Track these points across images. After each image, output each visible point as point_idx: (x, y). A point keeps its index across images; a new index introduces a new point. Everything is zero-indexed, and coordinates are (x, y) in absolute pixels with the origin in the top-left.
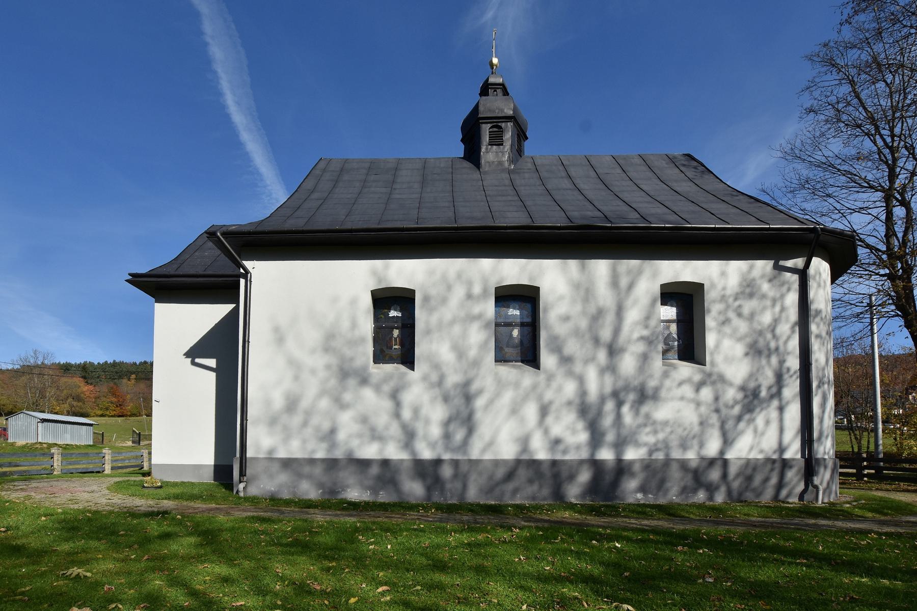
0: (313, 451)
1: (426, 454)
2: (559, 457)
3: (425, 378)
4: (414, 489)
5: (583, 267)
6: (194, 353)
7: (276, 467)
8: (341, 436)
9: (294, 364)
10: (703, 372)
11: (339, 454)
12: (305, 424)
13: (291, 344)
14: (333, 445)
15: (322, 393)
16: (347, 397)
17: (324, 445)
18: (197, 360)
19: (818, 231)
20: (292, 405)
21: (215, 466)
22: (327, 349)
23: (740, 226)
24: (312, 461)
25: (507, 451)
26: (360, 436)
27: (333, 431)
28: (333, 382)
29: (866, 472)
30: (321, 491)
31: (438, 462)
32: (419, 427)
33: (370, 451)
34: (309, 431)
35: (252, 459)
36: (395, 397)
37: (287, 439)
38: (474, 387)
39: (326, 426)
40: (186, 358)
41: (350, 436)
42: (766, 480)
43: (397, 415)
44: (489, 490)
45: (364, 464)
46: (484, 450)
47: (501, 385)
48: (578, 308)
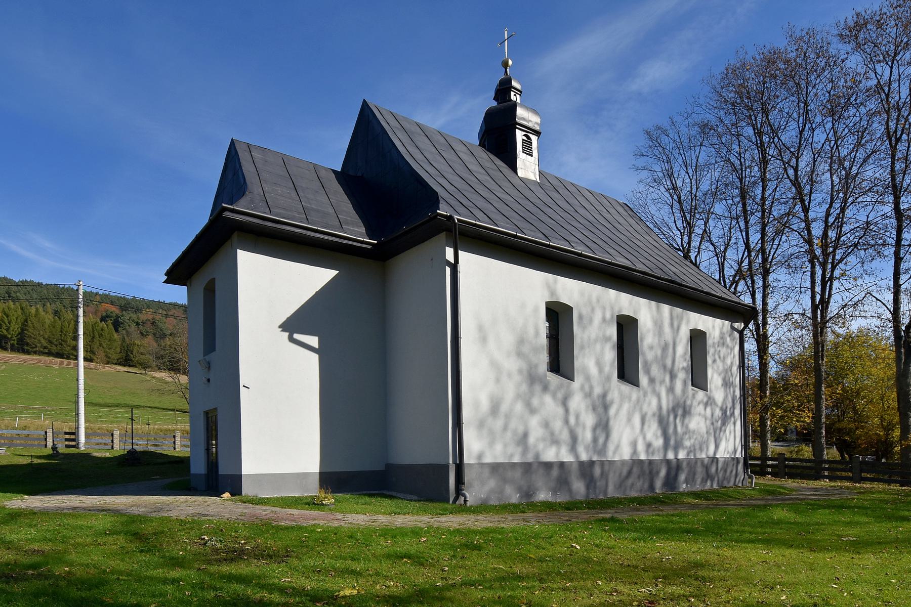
0: (512, 456)
1: (584, 457)
2: (651, 458)
3: (582, 388)
4: (579, 487)
5: (658, 308)
6: (293, 325)
7: (486, 472)
8: (531, 440)
9: (495, 365)
10: (707, 395)
11: (530, 458)
12: (505, 428)
13: (492, 344)
14: (526, 450)
15: (518, 396)
16: (535, 402)
17: (520, 449)
18: (297, 336)
19: (454, 220)
20: (495, 409)
21: (320, 473)
22: (520, 354)
23: (539, 240)
24: (513, 465)
25: (625, 454)
26: (544, 440)
27: (525, 435)
28: (524, 387)
29: (770, 463)
30: (518, 495)
31: (592, 463)
32: (579, 431)
33: (550, 455)
34: (509, 434)
35: (469, 464)
36: (564, 403)
37: (492, 443)
38: (609, 398)
39: (521, 429)
40: (282, 331)
41: (537, 440)
42: (732, 472)
43: (566, 421)
44: (621, 485)
45: (548, 466)
46: (614, 453)
47: (623, 398)
48: (656, 341)
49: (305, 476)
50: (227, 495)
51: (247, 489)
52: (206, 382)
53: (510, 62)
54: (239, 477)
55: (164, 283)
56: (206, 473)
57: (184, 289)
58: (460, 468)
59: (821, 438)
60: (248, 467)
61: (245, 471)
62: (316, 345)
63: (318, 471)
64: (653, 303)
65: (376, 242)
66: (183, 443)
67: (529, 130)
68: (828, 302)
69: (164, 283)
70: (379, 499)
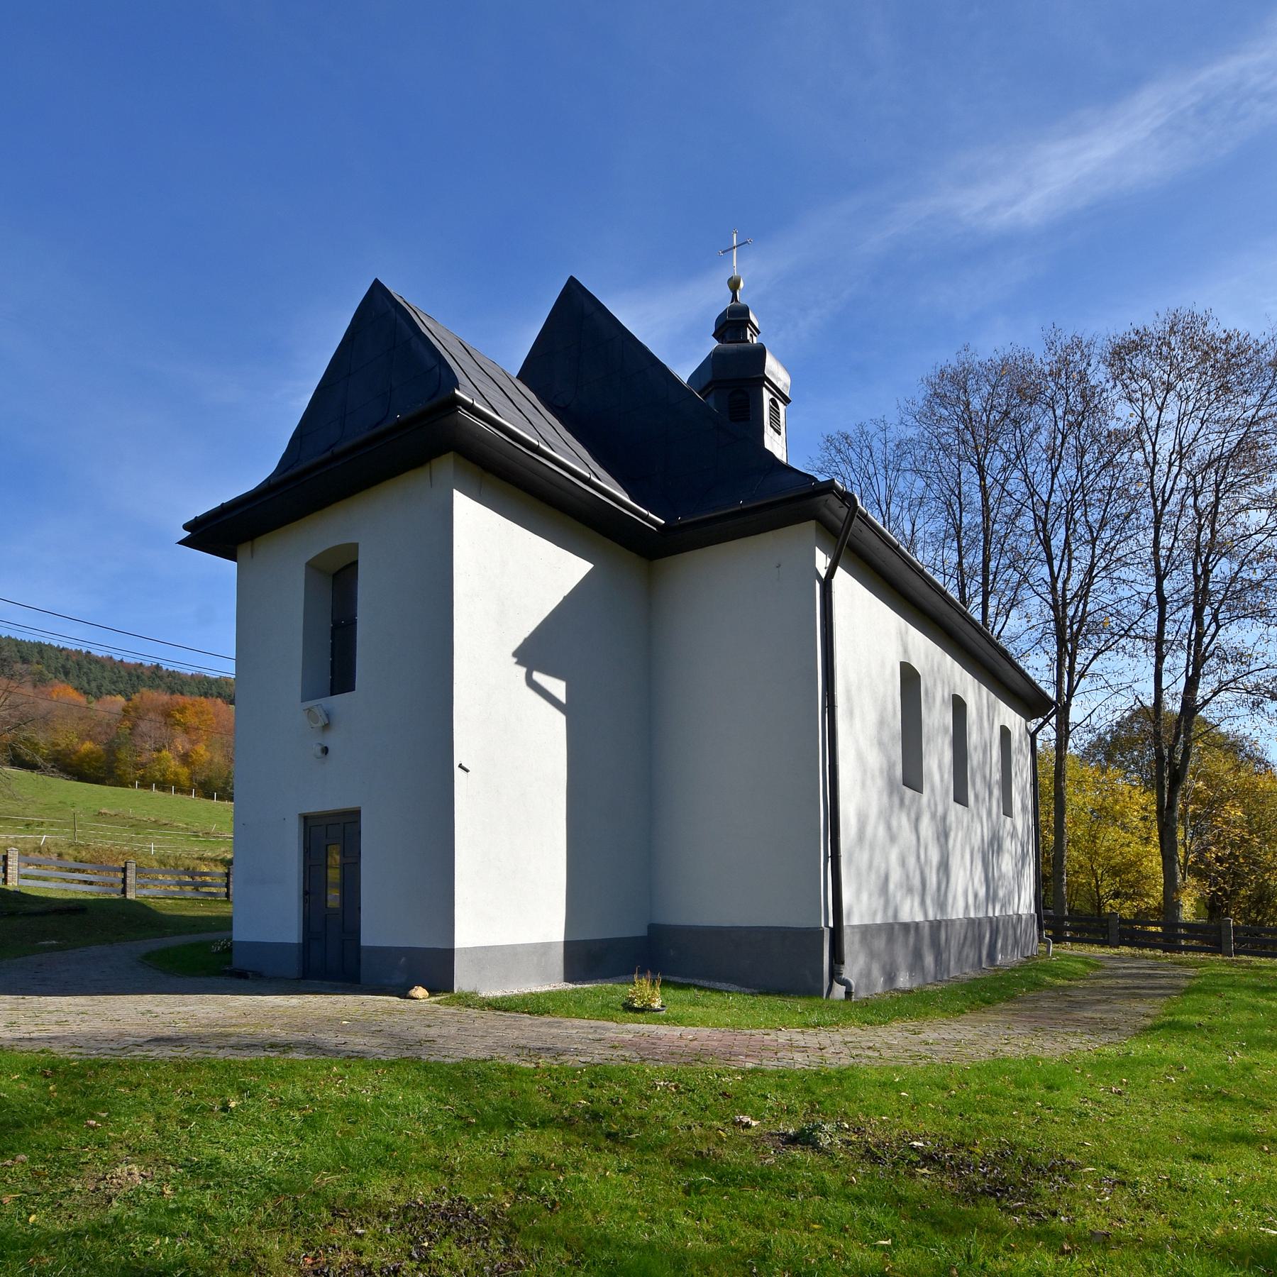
18: (538, 677)
49: (546, 947)
50: (420, 992)
51: (463, 981)
52: (319, 754)
53: (742, 285)
54: (448, 955)
55: (179, 543)
56: (301, 942)
57: (232, 565)
58: (837, 933)
59: (1062, 886)
60: (467, 935)
61: (457, 946)
62: (562, 696)
63: (563, 940)
64: (976, 681)
65: (663, 522)
66: (23, 871)
67: (778, 394)
68: (1068, 705)
69: (179, 543)
70: (672, 991)
